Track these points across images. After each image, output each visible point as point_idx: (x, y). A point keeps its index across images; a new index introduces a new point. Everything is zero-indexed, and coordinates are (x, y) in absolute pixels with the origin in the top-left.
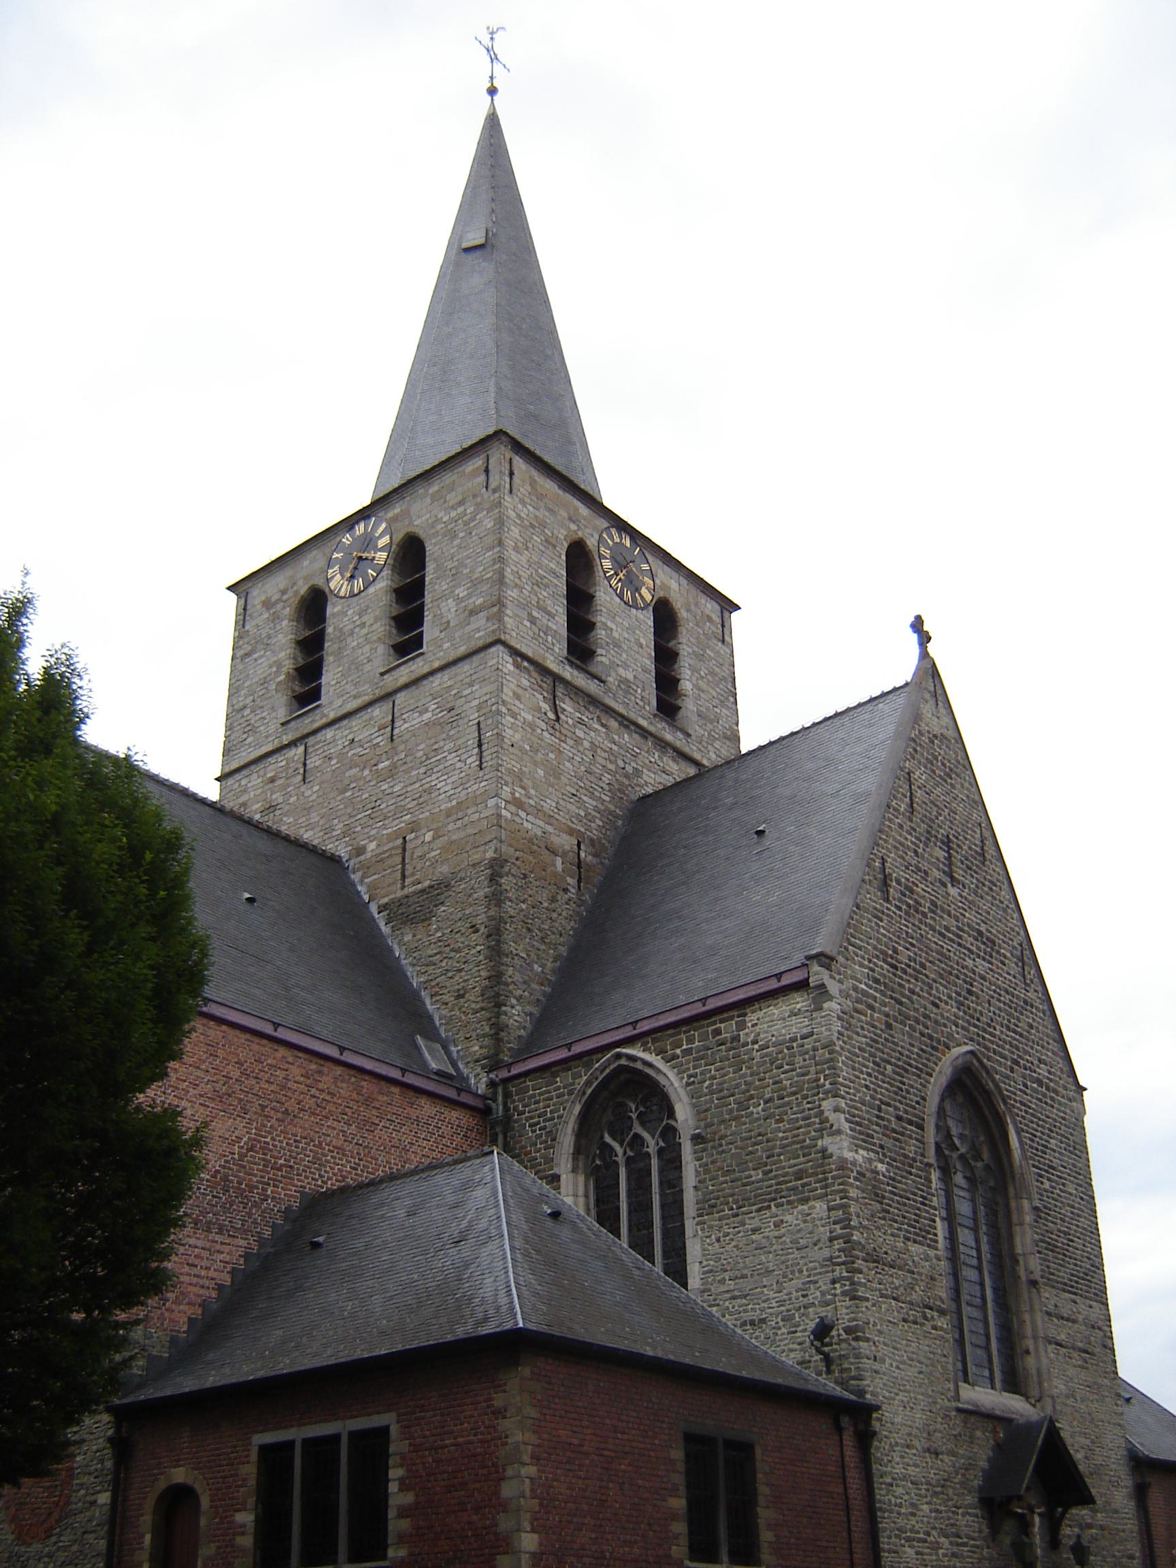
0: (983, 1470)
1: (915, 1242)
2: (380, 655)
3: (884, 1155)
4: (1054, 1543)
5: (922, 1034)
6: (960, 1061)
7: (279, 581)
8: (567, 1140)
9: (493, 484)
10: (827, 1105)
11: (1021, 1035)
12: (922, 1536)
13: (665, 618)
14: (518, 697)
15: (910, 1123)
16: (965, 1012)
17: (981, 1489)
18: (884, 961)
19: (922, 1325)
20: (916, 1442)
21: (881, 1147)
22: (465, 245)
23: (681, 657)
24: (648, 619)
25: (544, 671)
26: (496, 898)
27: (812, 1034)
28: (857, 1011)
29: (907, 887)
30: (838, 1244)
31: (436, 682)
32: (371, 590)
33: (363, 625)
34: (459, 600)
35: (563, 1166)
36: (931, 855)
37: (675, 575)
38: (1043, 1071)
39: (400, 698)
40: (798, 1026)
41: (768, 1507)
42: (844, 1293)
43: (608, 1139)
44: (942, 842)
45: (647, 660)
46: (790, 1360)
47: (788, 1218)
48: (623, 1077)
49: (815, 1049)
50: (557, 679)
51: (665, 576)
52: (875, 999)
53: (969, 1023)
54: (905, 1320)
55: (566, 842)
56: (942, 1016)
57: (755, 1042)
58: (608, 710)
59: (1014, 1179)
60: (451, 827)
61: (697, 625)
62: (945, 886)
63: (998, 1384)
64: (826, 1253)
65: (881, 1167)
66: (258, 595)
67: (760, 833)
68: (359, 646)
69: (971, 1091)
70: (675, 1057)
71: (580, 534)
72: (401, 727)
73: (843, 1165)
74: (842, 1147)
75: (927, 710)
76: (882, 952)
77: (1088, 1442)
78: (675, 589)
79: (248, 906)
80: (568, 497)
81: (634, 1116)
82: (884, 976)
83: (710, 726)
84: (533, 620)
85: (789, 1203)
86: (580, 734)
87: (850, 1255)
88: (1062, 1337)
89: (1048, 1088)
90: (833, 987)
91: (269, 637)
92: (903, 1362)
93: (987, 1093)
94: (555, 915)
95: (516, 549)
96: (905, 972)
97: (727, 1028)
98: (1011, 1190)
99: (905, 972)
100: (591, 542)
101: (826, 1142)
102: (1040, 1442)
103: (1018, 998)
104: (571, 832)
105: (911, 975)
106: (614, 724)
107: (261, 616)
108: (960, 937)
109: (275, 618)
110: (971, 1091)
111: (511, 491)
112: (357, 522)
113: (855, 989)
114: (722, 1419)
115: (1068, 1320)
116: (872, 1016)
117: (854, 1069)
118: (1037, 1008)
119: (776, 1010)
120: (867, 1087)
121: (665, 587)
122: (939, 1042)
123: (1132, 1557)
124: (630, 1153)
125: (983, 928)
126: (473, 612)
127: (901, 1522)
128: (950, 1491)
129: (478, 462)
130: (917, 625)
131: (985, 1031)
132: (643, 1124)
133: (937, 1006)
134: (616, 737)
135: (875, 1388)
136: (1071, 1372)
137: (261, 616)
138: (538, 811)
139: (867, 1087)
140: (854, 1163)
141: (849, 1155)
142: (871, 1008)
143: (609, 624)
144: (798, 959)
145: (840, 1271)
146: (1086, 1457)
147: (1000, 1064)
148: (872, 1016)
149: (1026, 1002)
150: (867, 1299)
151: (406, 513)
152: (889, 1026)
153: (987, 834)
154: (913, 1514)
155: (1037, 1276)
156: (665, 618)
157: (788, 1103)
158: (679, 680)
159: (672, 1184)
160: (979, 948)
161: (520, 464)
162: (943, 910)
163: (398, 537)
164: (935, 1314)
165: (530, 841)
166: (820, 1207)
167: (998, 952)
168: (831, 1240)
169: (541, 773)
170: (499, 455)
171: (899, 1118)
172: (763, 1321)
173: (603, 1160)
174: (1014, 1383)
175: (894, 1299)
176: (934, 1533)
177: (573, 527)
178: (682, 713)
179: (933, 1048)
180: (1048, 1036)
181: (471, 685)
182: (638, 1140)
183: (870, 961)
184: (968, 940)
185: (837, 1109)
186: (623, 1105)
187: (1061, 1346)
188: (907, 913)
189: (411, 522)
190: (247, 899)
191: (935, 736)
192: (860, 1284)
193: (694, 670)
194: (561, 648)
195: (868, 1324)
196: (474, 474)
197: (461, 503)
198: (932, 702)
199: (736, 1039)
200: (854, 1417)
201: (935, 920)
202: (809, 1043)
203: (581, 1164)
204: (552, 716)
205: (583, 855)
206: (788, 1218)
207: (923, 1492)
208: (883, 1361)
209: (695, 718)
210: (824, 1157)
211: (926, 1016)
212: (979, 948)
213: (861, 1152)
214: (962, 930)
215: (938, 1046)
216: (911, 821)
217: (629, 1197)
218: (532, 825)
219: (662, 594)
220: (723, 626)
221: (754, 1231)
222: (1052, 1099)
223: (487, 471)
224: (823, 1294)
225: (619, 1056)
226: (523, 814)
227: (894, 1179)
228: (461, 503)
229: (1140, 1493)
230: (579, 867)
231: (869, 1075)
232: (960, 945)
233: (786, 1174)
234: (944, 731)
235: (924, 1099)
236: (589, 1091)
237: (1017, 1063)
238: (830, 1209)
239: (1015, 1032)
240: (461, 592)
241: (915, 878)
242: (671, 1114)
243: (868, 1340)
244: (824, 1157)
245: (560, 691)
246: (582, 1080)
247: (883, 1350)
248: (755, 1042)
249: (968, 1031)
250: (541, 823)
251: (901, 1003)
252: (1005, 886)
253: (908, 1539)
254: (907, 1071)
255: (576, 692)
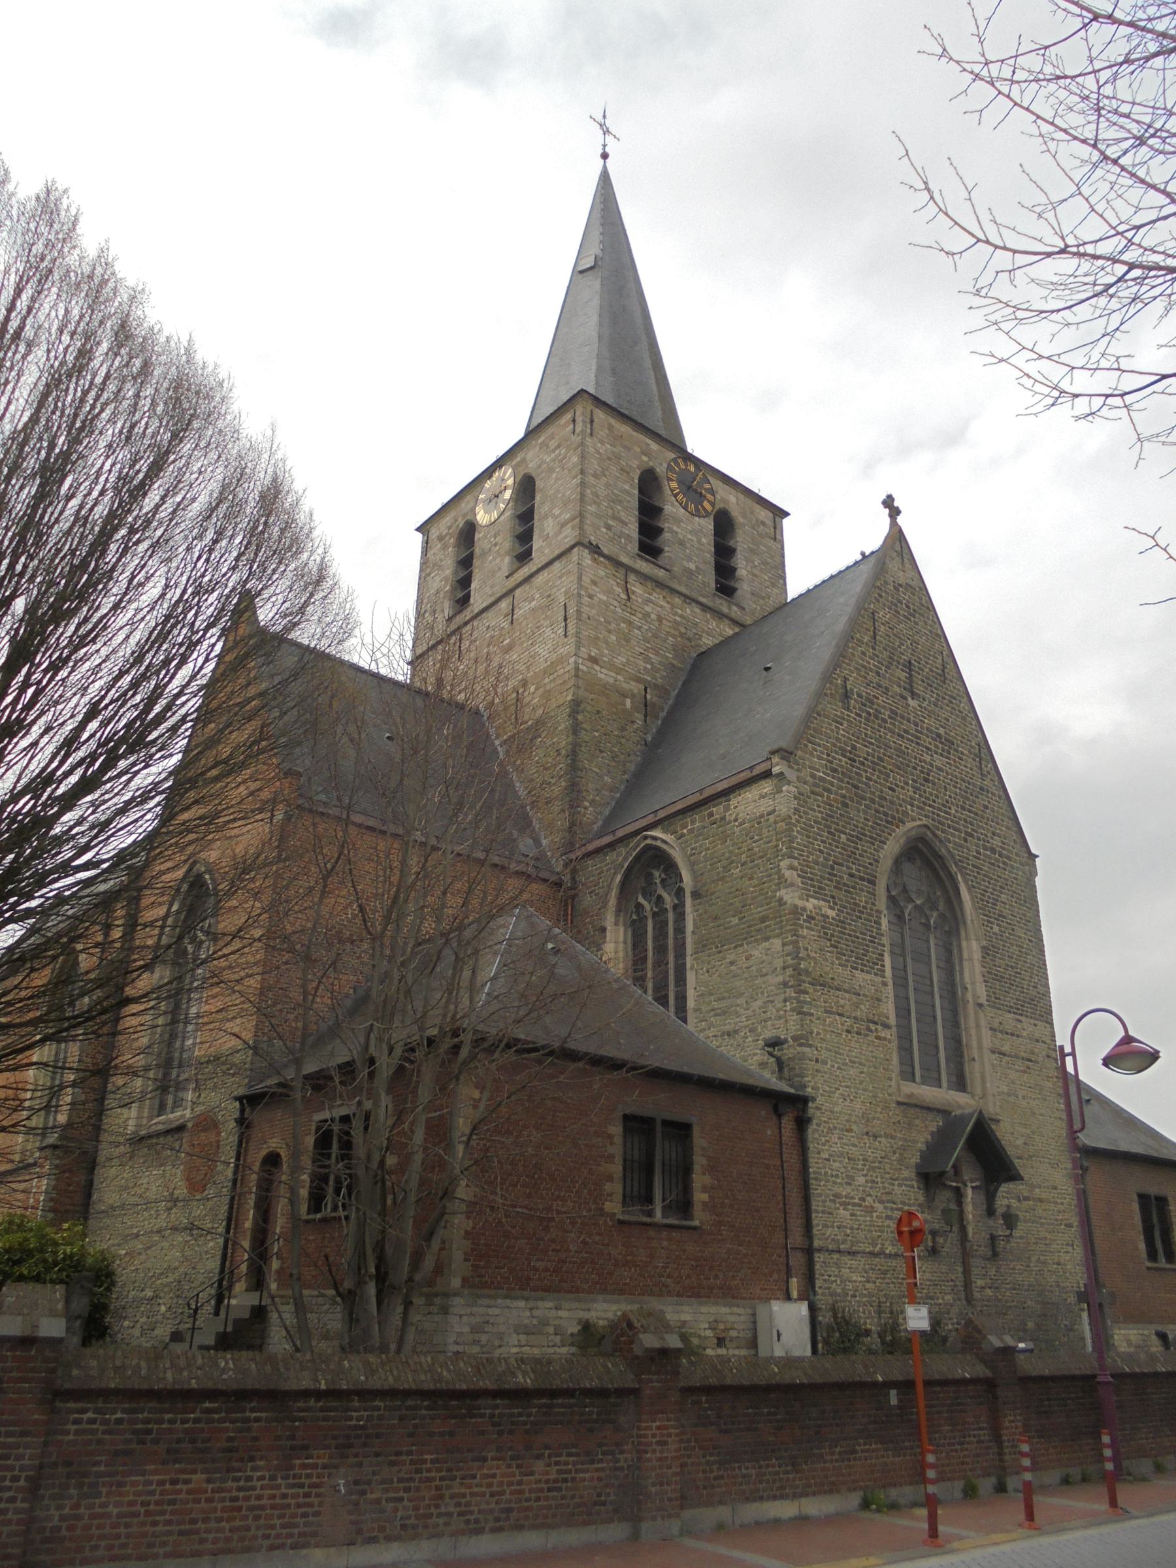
0: (921, 1151)
1: (862, 971)
2: (506, 562)
3: (835, 903)
4: (990, 1212)
5: (877, 811)
6: (913, 832)
7: (447, 520)
8: (613, 901)
9: (578, 430)
10: (784, 864)
11: (976, 814)
12: (856, 1201)
13: (724, 525)
14: (594, 583)
15: (862, 879)
16: (920, 795)
17: (918, 1166)
18: (843, 755)
19: (867, 1035)
20: (854, 1127)
21: (833, 897)
22: (580, 269)
23: (738, 552)
24: (708, 525)
25: (618, 564)
26: (575, 729)
27: (774, 811)
28: (813, 793)
29: (868, 700)
30: (789, 971)
31: (540, 579)
32: (502, 518)
33: (496, 545)
34: (555, 517)
35: (609, 920)
36: (892, 675)
37: (734, 492)
38: (996, 842)
39: (518, 592)
40: (765, 806)
41: (704, 1174)
42: (792, 1010)
43: (641, 900)
44: (904, 666)
45: (709, 555)
46: (753, 1063)
47: (756, 953)
48: (650, 853)
49: (776, 822)
50: (629, 569)
51: (722, 491)
52: (832, 784)
53: (925, 804)
54: (848, 1031)
55: (637, 688)
56: (898, 798)
57: (736, 820)
58: (673, 591)
59: (965, 923)
60: (547, 680)
61: (753, 528)
62: (906, 699)
63: (944, 1084)
64: (780, 979)
65: (832, 913)
66: (434, 533)
67: (767, 669)
68: (494, 559)
69: (922, 853)
70: (683, 835)
71: (651, 464)
72: (518, 613)
73: (796, 911)
74: (790, 897)
75: (893, 565)
76: (840, 748)
77: (1028, 1131)
78: (732, 501)
79: (389, 742)
80: (641, 437)
81: (658, 881)
82: (842, 766)
83: (762, 602)
84: (609, 527)
85: (756, 941)
86: (648, 609)
87: (800, 979)
88: (1006, 1048)
89: (1001, 855)
90: (791, 775)
91: (441, 560)
92: (844, 1064)
93: (940, 857)
94: (623, 741)
95: (595, 476)
96: (863, 764)
97: (717, 810)
98: (963, 933)
99: (863, 764)
100: (661, 470)
101: (782, 893)
102: (969, 1128)
103: (974, 785)
104: (638, 680)
105: (869, 767)
106: (677, 600)
107: (436, 547)
108: (919, 738)
109: (445, 547)
110: (922, 853)
111: (591, 434)
112: (494, 471)
113: (813, 776)
114: (659, 1104)
115: (1012, 1035)
116: (828, 798)
117: (808, 837)
118: (993, 794)
119: (750, 795)
120: (820, 851)
121: (727, 502)
122: (894, 818)
123: (1069, 1226)
124: (656, 910)
125: (942, 731)
126: (563, 525)
127: (836, 1189)
128: (887, 1167)
129: (569, 416)
130: (889, 502)
131: (939, 809)
132: (664, 887)
133: (893, 790)
134: (679, 611)
135: (816, 1085)
136: (1013, 1075)
137: (436, 547)
138: (612, 667)
139: (820, 851)
140: (804, 909)
141: (800, 903)
142: (829, 791)
143: (675, 528)
144: (765, 754)
145: (791, 993)
146: (1025, 1144)
147: (953, 835)
148: (828, 798)
149: (982, 789)
150: (812, 1015)
151: (524, 461)
152: (846, 805)
153: (949, 660)
154: (850, 1184)
155: (983, 1000)
156: (724, 525)
157: (757, 865)
158: (735, 569)
159: (680, 930)
160: (936, 746)
161: (600, 415)
162: (902, 717)
163: (520, 477)
164: (880, 1028)
165: (604, 686)
166: (776, 943)
167: (956, 750)
168: (784, 968)
169: (614, 638)
170: (581, 410)
171: (851, 875)
172: (736, 1032)
173: (638, 915)
174: (960, 1083)
175: (839, 1014)
176: (869, 1198)
177: (645, 458)
178: (739, 593)
179: (887, 822)
180: (1003, 814)
181: (560, 577)
182: (660, 899)
183: (828, 755)
184: (926, 741)
185: (791, 867)
186: (652, 874)
187: (1004, 1055)
188: (866, 719)
189: (527, 466)
190: (388, 738)
191: (900, 585)
192: (805, 1002)
193: (747, 560)
194: (634, 547)
195: (811, 1033)
196: (565, 426)
197: (558, 446)
198: (898, 560)
199: (723, 818)
200: (792, 1107)
201: (894, 725)
202: (772, 818)
203: (621, 920)
204: (624, 596)
205: (649, 696)
206: (756, 953)
207: (860, 1166)
208: (826, 1063)
209: (748, 596)
210: (780, 905)
211: (882, 798)
212: (936, 746)
213: (811, 900)
214: (921, 733)
215: (895, 821)
216: (874, 649)
217: (654, 942)
218: (604, 675)
219: (722, 505)
220: (775, 528)
221: (732, 963)
222: (1004, 863)
223: (574, 421)
224: (778, 1010)
225: (646, 837)
226: (597, 668)
227: (842, 922)
228: (558, 446)
229: (1080, 1175)
230: (646, 705)
231: (823, 842)
232: (918, 744)
233: (754, 919)
234: (911, 583)
235: (877, 861)
236: (626, 865)
237: (972, 836)
238: (784, 945)
239: (970, 811)
240: (557, 511)
241: (875, 692)
242: (681, 881)
243: (810, 1046)
244: (780, 905)
245: (632, 578)
246: (623, 857)
247: (824, 1054)
248: (736, 820)
249: (923, 809)
250: (614, 675)
251: (857, 787)
252: (965, 699)
253: (842, 1204)
254: (861, 840)
255: (644, 578)
